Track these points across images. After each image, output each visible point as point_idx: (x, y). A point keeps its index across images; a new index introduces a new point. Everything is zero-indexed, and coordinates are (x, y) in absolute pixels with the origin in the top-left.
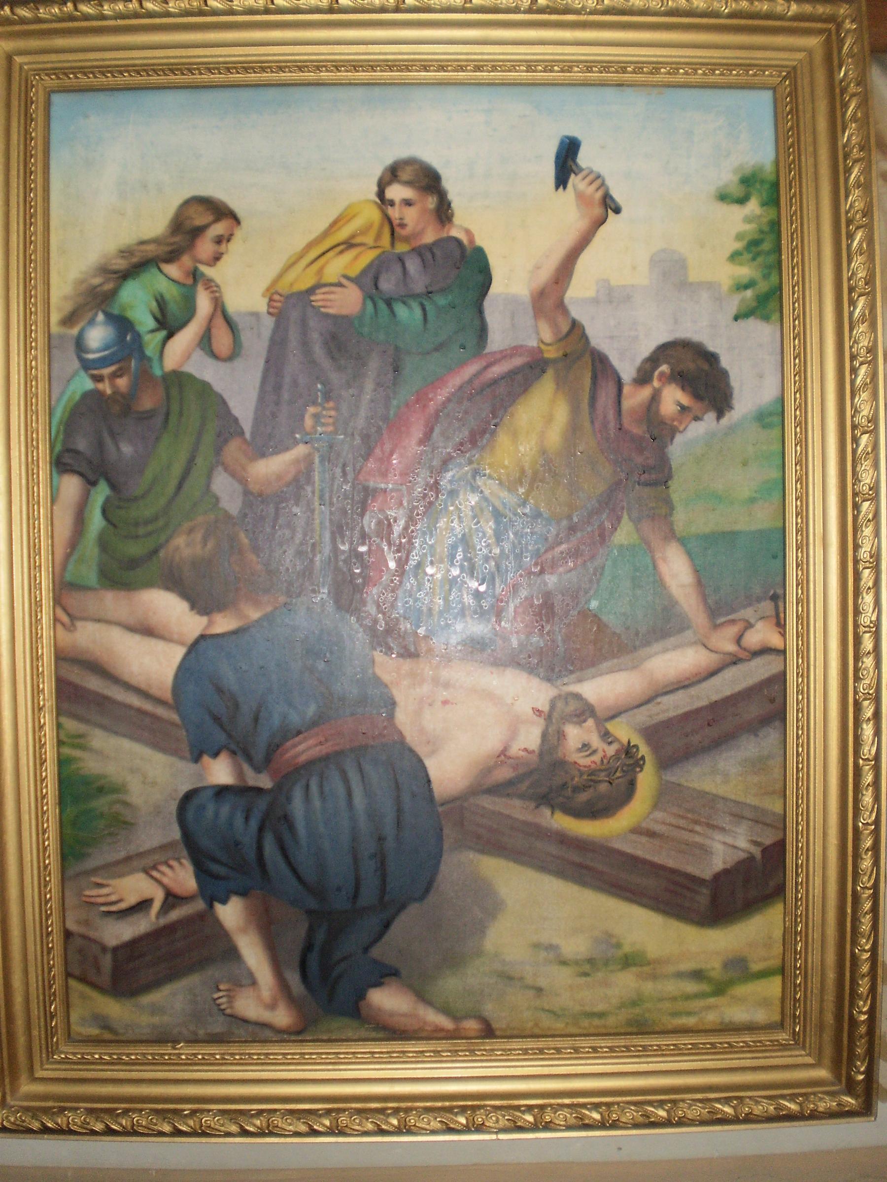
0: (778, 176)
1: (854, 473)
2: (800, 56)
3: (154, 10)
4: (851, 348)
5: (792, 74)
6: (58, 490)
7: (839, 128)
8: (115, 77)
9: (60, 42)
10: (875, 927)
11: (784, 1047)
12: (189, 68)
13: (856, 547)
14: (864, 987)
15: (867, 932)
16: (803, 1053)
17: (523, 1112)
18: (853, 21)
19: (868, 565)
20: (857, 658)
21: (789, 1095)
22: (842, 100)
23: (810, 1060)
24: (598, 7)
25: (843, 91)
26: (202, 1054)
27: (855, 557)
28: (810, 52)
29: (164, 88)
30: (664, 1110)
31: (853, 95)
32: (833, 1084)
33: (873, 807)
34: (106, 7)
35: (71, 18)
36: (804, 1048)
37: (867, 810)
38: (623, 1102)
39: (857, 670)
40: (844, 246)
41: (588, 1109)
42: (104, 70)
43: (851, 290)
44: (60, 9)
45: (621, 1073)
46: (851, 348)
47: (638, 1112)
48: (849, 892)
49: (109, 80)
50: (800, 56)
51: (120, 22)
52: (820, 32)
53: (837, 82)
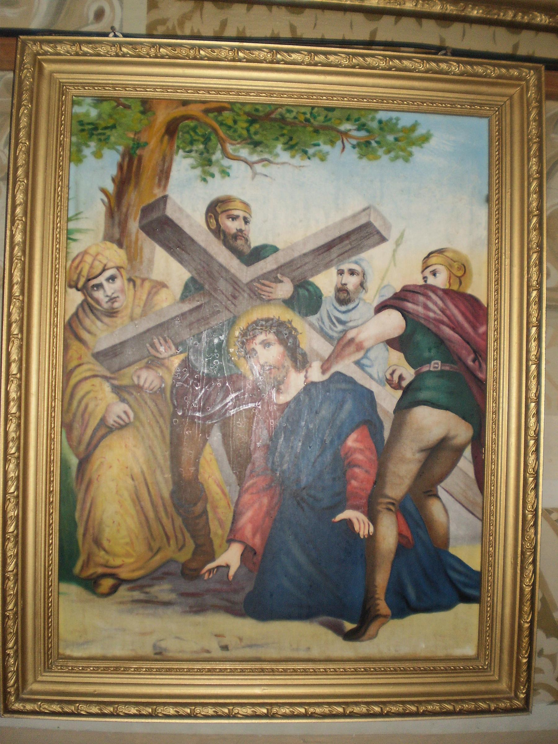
3: (299, 707)
5: (48, 668)
9: (463, 688)
11: (75, 85)
12: (416, 671)
13: (21, 347)
16: (61, 80)
20: (22, 319)
21: (48, 55)
24: (194, 708)
26: (433, 106)
28: (36, 681)
29: (390, 660)
30: (123, 52)
31: (10, 648)
34: (401, 708)
36: (60, 82)
38: (225, 61)
41: (129, 54)
42: (405, 671)
45: (128, 75)
47: (139, 51)
49: (402, 665)
50: (40, 678)
51: (463, 698)
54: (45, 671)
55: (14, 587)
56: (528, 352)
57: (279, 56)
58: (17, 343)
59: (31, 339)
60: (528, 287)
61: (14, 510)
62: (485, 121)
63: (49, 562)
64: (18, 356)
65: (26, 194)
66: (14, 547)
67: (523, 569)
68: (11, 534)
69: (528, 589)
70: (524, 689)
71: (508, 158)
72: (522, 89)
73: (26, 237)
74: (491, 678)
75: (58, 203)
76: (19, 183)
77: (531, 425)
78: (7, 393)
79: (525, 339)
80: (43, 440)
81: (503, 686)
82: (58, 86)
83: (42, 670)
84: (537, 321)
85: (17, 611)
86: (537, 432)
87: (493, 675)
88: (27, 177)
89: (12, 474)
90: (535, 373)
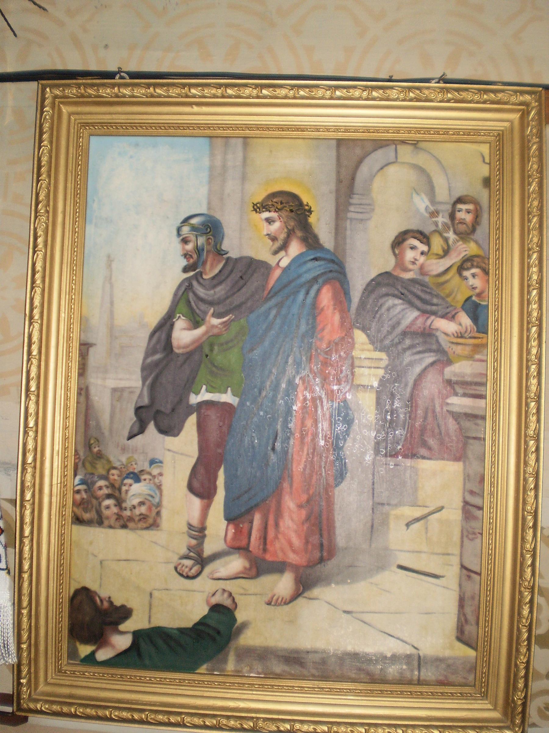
0: (476, 662)
1: (524, 500)
2: (507, 124)
4: (528, 244)
6: (22, 585)
7: (526, 125)
8: (108, 129)
10: (540, 149)
13: (527, 427)
14: (521, 685)
15: (526, 616)
17: (378, 97)
18: (536, 102)
19: (534, 324)
20: (523, 530)
22: (528, 146)
23: (491, 708)
25: (529, 141)
27: (525, 434)
28: (511, 121)
31: (534, 143)
32: (503, 722)
33: (532, 541)
35: (82, 96)
37: (528, 542)
39: (524, 500)
40: (526, 298)
43: (529, 286)
44: (76, 91)
46: (528, 244)
48: (515, 627)
50: (507, 124)
52: (518, 111)
53: (350, 385)
54: (502, 131)
55: (532, 274)
56: (39, 366)
57: (485, 96)
58: (530, 470)
59: (519, 321)
60: (35, 467)
61: (532, 310)
62: (93, 139)
63: (499, 212)
64: (526, 533)
65: (520, 614)
66: (531, 312)
67: (48, 196)
68: (536, 250)
69: (44, 176)
70: (46, 116)
71: (50, 626)
72: (62, 103)
73: (519, 610)
74: (77, 117)
75: (491, 572)
76: (527, 625)
77: (33, 405)
78: (540, 346)
79: (39, 451)
80: (507, 167)
81: (42, 687)
82: (489, 695)
83: (505, 132)
84: (27, 469)
85: (528, 215)
86: (27, 435)
87: (47, 683)
88: (519, 630)
89: (535, 306)
90: (30, 418)
